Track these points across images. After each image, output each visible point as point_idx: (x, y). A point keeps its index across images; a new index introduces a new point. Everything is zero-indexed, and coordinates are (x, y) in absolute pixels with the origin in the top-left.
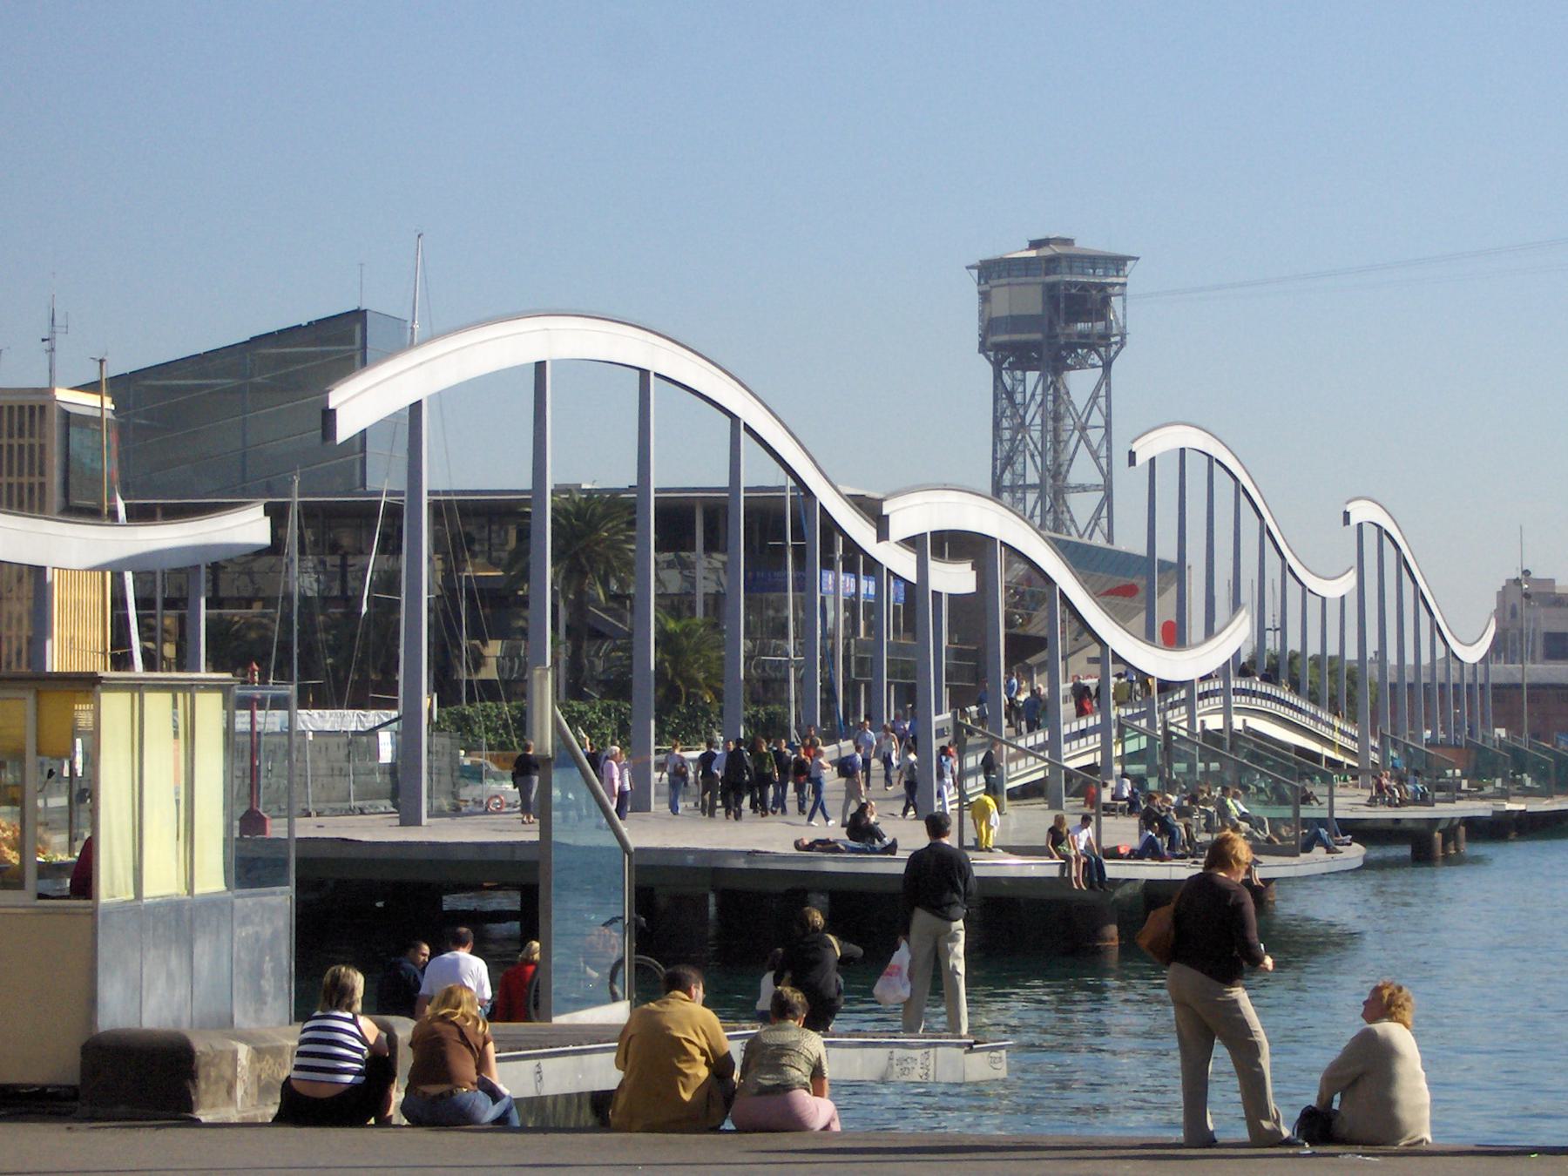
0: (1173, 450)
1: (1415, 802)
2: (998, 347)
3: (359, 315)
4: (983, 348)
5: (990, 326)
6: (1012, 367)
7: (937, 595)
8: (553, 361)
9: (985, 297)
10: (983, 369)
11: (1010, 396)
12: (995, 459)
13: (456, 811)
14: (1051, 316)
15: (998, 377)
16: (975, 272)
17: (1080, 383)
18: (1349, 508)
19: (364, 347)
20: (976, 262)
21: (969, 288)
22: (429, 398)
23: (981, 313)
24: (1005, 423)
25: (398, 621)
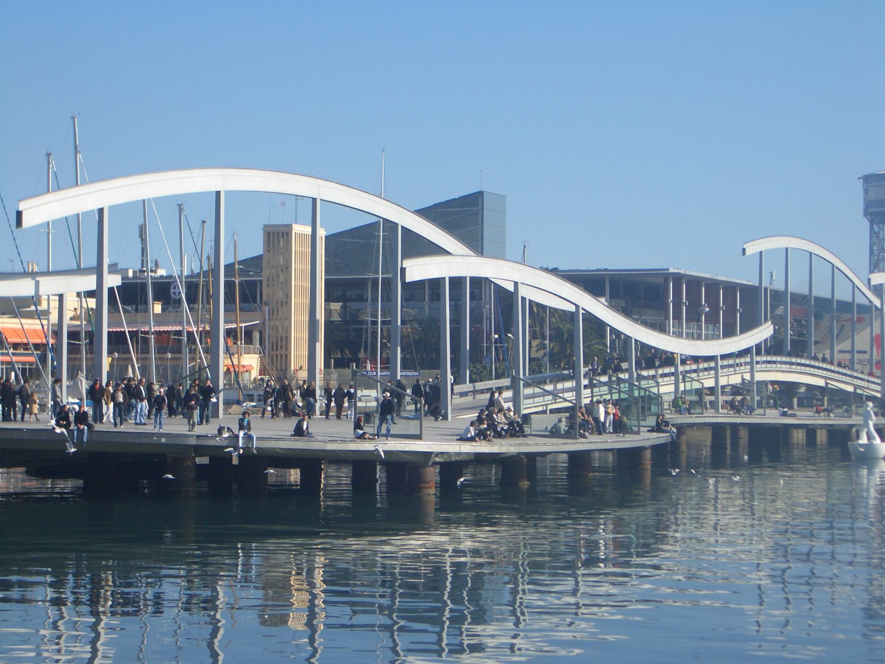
0: (137, 202)
1: (668, 359)
2: (871, 214)
3: (480, 194)
4: (865, 214)
5: (868, 205)
6: (878, 223)
7: (523, 299)
8: (227, 192)
9: (866, 191)
10: (865, 224)
11: (878, 237)
12: (870, 264)
13: (361, 437)
15: (872, 228)
16: (862, 181)
18: (22, 206)
19: (483, 208)
20: (861, 175)
21: (858, 188)
22: (110, 208)
23: (865, 199)
24: (875, 248)
25: (451, 354)
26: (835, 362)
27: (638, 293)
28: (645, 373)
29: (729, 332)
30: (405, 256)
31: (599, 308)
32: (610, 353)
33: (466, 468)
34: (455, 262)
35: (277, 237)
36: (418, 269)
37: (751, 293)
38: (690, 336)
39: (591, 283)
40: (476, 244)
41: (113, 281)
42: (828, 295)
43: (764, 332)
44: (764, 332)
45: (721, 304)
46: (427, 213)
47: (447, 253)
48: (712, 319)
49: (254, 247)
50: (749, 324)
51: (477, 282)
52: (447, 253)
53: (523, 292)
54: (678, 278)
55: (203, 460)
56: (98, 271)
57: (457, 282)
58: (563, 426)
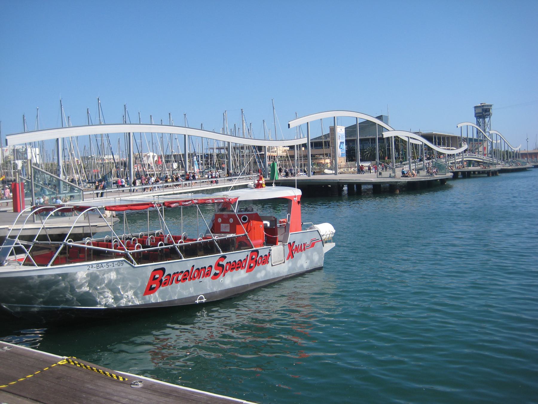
14: (483, 113)
17: (487, 120)
27: (440, 140)
35: (333, 130)
49: (327, 131)
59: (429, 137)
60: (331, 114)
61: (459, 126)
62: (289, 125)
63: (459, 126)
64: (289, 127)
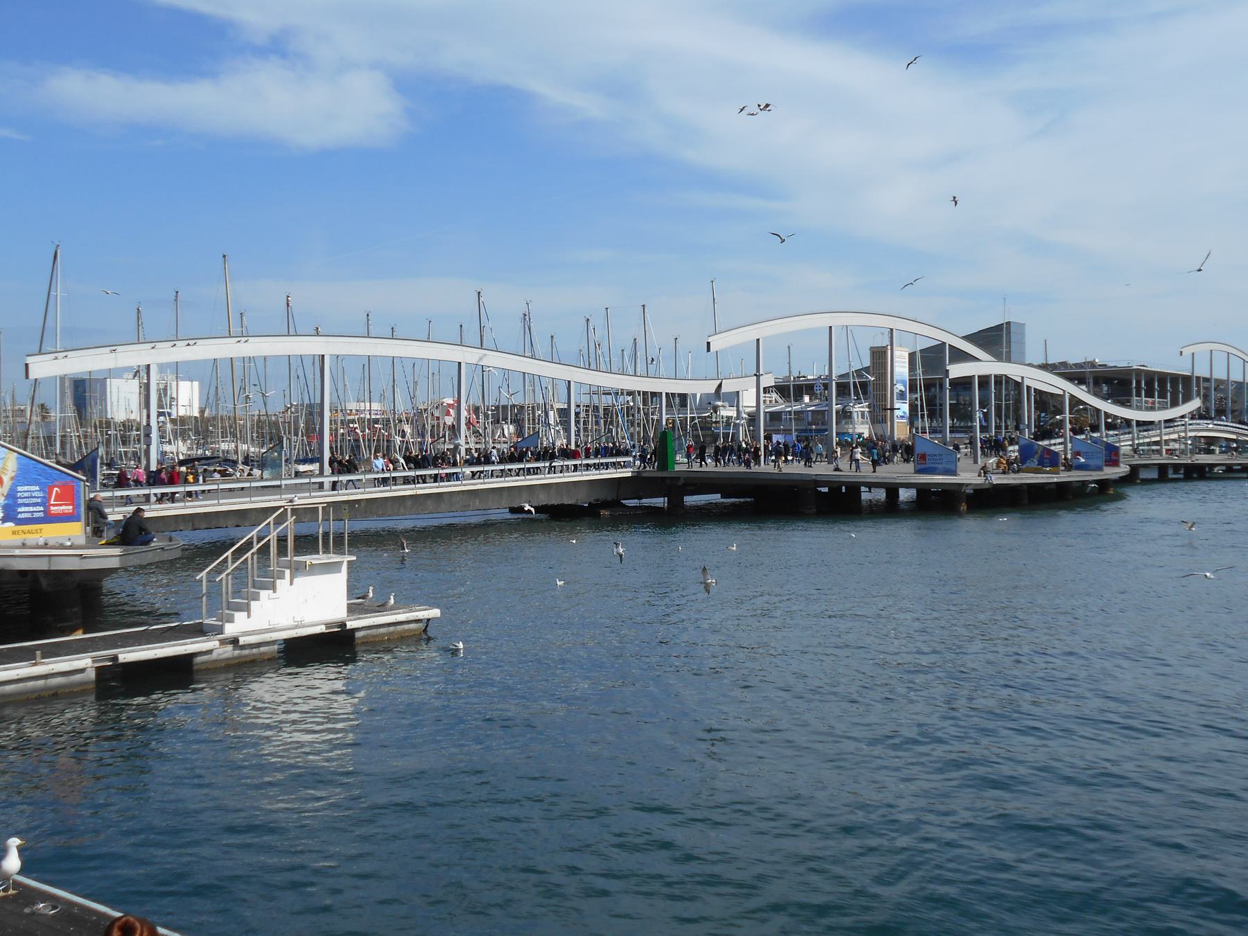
3: (999, 328)
26: (541, 347)
27: (1118, 384)
28: (1111, 433)
29: (1174, 404)
30: (951, 362)
31: (1081, 393)
32: (1086, 421)
33: (878, 501)
34: (985, 365)
35: (880, 356)
36: (957, 371)
37: (1187, 380)
38: (1147, 409)
39: (1075, 375)
40: (999, 357)
41: (767, 381)
42: (1224, 377)
43: (1196, 404)
44: (1196, 404)
45: (1168, 387)
46: (969, 338)
47: (977, 359)
48: (1162, 395)
50: (1187, 399)
51: (999, 379)
52: (977, 359)
53: (1027, 382)
54: (1138, 372)
55: (825, 490)
56: (758, 376)
57: (984, 381)
58: (1170, 471)
59: (1075, 375)
60: (824, 321)
61: (1187, 352)
62: (708, 344)
63: (1187, 352)
64: (708, 350)
